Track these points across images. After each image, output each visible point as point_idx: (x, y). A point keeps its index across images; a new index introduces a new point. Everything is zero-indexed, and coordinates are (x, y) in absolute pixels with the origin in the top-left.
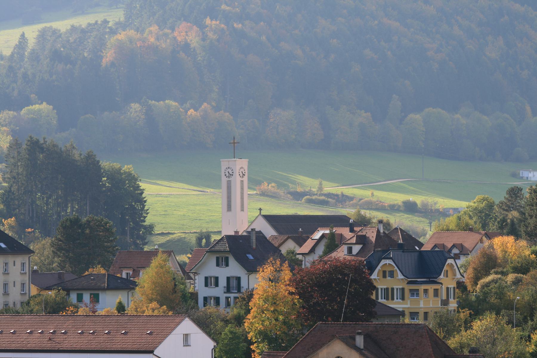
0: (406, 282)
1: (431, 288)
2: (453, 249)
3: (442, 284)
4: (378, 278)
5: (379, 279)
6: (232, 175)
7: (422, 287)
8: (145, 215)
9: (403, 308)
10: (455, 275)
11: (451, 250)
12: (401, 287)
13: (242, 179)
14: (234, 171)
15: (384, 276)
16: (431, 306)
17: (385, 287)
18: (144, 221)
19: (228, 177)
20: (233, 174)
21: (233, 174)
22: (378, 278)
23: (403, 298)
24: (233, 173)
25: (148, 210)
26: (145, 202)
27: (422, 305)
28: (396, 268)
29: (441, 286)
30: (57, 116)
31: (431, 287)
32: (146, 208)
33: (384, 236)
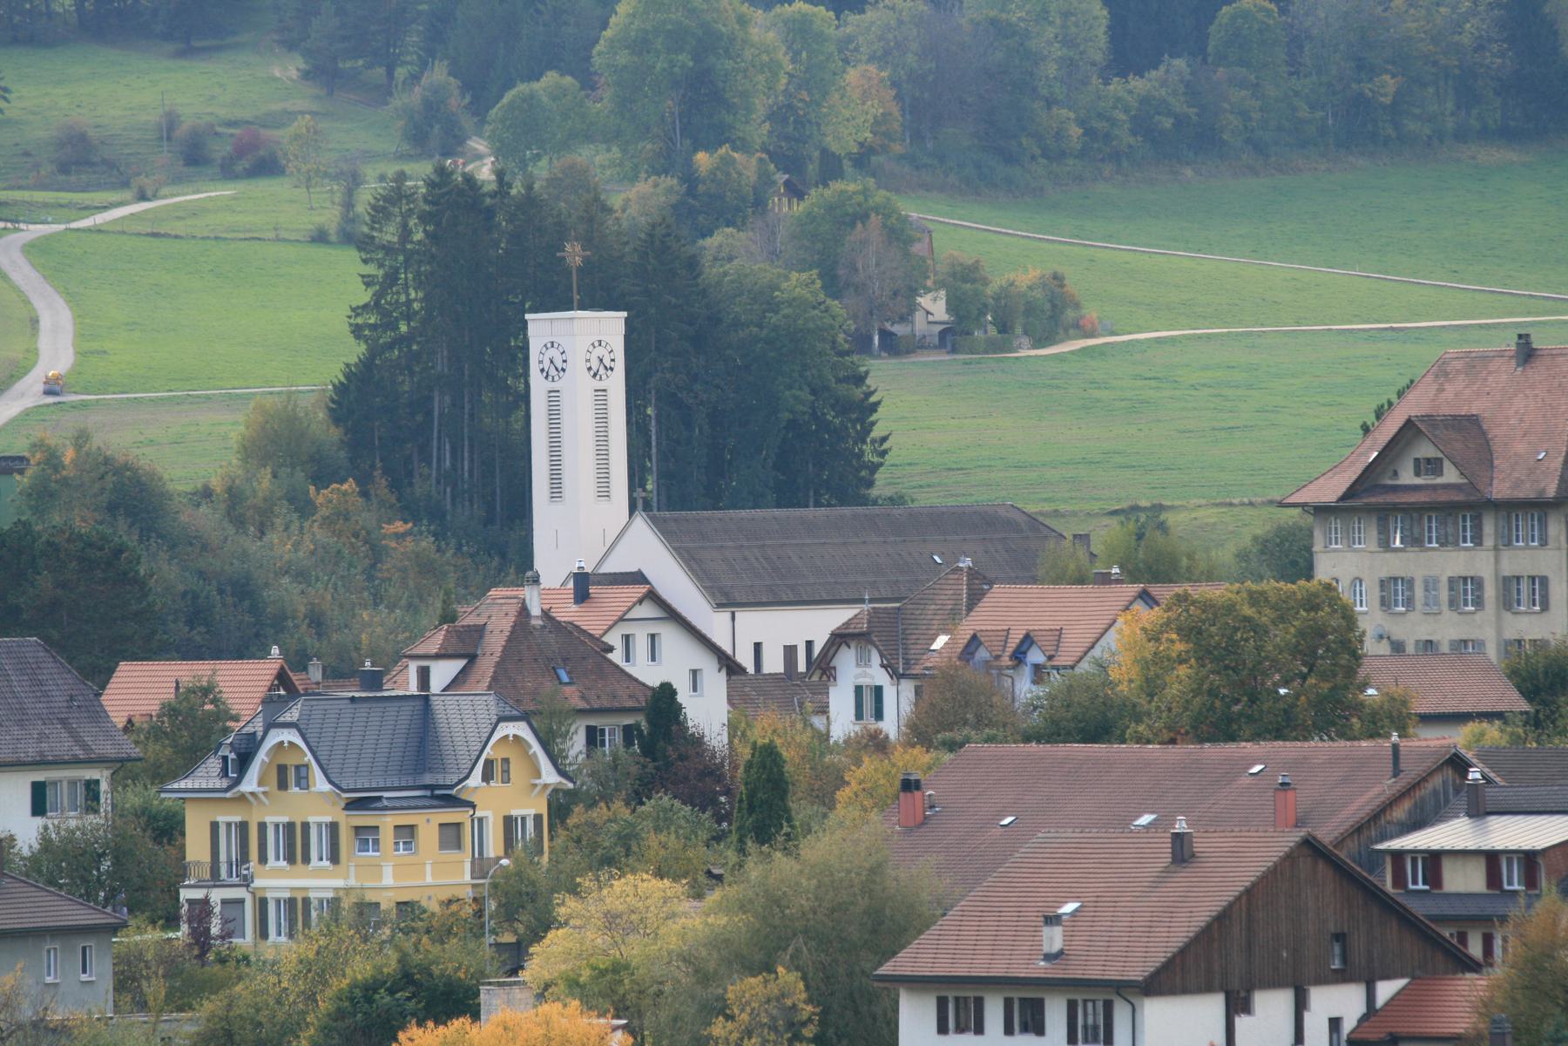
0: (343, 804)
1: (428, 821)
2: (1029, 648)
3: (473, 806)
4: (262, 789)
5: (264, 793)
6: (612, 369)
7: (388, 819)
8: (876, 459)
9: (292, 889)
10: (538, 774)
11: (1025, 653)
12: (328, 819)
13: (601, 385)
14: (568, 356)
15: (283, 785)
16: (429, 880)
17: (285, 819)
18: (870, 484)
19: (592, 373)
20: (612, 364)
21: (564, 366)
22: (262, 789)
23: (335, 858)
24: (565, 361)
25: (884, 439)
26: (874, 407)
27: (388, 880)
28: (309, 757)
29: (471, 812)
30: (1105, 12)
31: (427, 817)
32: (877, 433)
33: (543, 627)
